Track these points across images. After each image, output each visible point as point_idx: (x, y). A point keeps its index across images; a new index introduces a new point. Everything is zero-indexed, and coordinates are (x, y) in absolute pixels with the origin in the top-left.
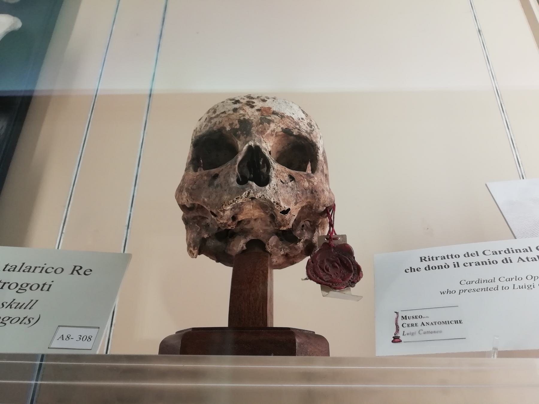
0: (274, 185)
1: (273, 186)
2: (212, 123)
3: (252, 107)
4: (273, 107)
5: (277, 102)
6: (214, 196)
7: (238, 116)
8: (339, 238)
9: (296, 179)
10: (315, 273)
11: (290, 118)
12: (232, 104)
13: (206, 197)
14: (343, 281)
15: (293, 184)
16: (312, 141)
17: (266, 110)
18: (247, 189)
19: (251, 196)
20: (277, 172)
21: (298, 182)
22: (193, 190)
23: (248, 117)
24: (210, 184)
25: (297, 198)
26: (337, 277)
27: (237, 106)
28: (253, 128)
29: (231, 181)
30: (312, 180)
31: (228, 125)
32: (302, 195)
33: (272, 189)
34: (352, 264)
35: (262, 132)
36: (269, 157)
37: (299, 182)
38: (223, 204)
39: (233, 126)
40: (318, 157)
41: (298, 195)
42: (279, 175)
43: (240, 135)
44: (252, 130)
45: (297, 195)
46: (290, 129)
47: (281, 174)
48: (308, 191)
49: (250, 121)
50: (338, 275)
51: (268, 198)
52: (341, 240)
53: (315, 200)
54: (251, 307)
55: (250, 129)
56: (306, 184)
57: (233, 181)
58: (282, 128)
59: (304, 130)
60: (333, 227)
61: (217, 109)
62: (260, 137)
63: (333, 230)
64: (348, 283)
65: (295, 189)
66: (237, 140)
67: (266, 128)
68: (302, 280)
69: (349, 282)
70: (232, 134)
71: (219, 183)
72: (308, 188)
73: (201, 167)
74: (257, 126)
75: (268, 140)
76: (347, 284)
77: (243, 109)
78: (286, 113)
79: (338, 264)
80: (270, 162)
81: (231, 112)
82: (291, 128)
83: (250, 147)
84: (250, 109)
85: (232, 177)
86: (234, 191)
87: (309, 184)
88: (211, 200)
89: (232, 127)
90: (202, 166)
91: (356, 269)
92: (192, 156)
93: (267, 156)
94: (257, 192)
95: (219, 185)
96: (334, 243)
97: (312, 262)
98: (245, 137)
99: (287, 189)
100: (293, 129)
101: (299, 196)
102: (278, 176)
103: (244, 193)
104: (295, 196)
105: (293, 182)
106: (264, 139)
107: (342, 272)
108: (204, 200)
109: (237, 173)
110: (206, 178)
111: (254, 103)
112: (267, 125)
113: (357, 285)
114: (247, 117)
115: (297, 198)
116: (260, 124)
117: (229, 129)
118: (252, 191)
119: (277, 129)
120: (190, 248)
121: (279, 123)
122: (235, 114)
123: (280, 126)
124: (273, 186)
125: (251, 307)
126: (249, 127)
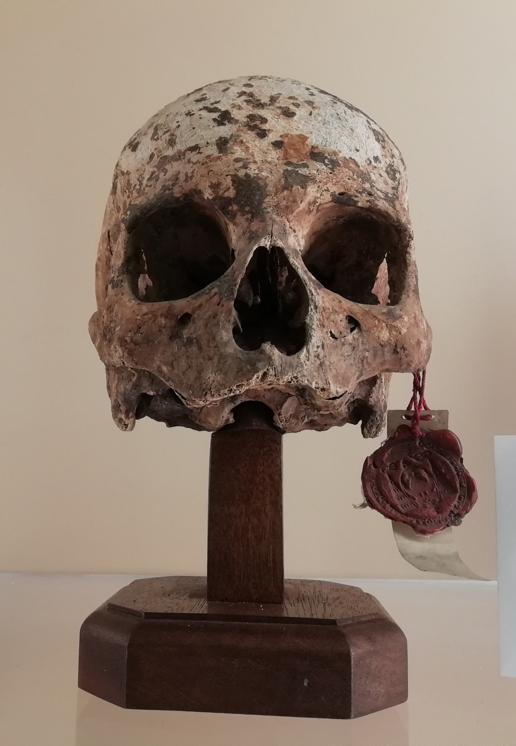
0: (318, 347)
1: (315, 349)
2: (169, 175)
3: (262, 134)
4: (311, 133)
5: (320, 118)
6: (183, 363)
7: (232, 168)
8: (433, 417)
9: (362, 325)
10: (381, 494)
11: (351, 165)
12: (212, 123)
13: (166, 364)
14: (438, 513)
15: (355, 336)
16: (399, 221)
17: (294, 145)
18: (260, 365)
19: (270, 381)
20: (322, 315)
21: (368, 331)
22: (136, 345)
23: (257, 172)
24: (174, 336)
25: (363, 366)
26: (425, 501)
27: (226, 130)
28: (266, 200)
29: (222, 339)
30: (398, 324)
31: (207, 187)
32: (372, 358)
33: (312, 358)
34: (458, 474)
35: (288, 209)
36: (306, 278)
37: (370, 332)
38: (206, 393)
39: (221, 192)
40: (407, 255)
41: (365, 361)
42: (328, 319)
43: (236, 214)
44: (264, 205)
45: (362, 361)
46: (352, 196)
47: (332, 317)
48: (386, 349)
49: (260, 182)
50: (428, 498)
51: (306, 382)
52: (436, 420)
53: (401, 366)
54: (251, 553)
55: (261, 202)
56: (385, 335)
57: (227, 338)
58: (333, 195)
59: (381, 191)
60: (421, 394)
61: (177, 133)
62: (283, 221)
63: (422, 401)
64: (447, 517)
65: (361, 348)
66: (228, 222)
67: (298, 199)
68: (355, 507)
69: (450, 515)
70: (216, 207)
71: (194, 337)
72: (387, 341)
73: (143, 272)
74: (276, 194)
75: (300, 224)
76: (446, 520)
77: (242, 142)
78: (340, 152)
79: (426, 471)
80: (308, 291)
81: (213, 151)
82: (352, 193)
83: (261, 250)
84: (258, 142)
85: (224, 328)
86: (230, 365)
87: (390, 334)
88: (176, 372)
89: (218, 193)
90: (146, 268)
91: (465, 485)
92: (125, 253)
93: (300, 275)
94: (283, 373)
95: (195, 340)
96: (422, 425)
97: (375, 466)
98: (247, 219)
99: (343, 349)
100: (358, 194)
101: (367, 362)
102: (326, 323)
103: (255, 376)
104: (359, 363)
105: (355, 331)
106: (292, 224)
107: (435, 490)
108: (159, 367)
109: (235, 319)
110: (163, 321)
111: (264, 120)
112: (301, 190)
113: (466, 519)
114: (253, 170)
115: (363, 366)
116: (285, 188)
117: (211, 197)
118: (272, 372)
119: (322, 197)
120: (120, 414)
121: (326, 184)
122: (224, 158)
123: (327, 190)
124: (315, 349)
125: (251, 553)
126: (257, 198)
